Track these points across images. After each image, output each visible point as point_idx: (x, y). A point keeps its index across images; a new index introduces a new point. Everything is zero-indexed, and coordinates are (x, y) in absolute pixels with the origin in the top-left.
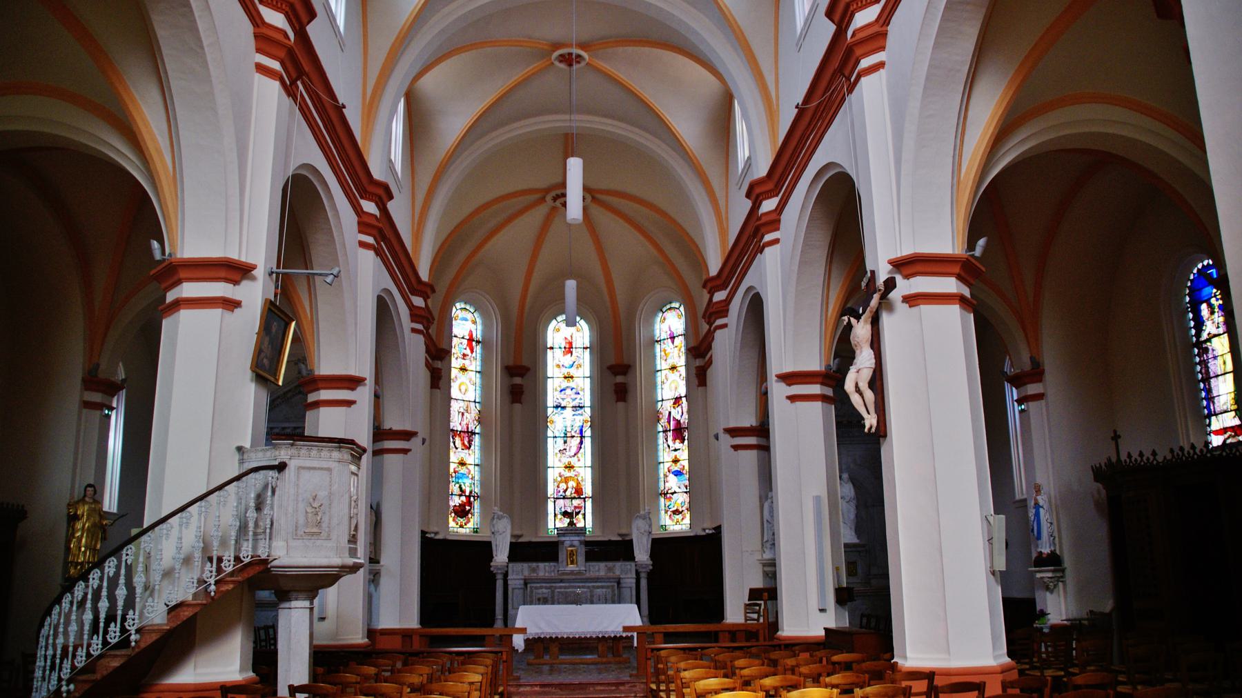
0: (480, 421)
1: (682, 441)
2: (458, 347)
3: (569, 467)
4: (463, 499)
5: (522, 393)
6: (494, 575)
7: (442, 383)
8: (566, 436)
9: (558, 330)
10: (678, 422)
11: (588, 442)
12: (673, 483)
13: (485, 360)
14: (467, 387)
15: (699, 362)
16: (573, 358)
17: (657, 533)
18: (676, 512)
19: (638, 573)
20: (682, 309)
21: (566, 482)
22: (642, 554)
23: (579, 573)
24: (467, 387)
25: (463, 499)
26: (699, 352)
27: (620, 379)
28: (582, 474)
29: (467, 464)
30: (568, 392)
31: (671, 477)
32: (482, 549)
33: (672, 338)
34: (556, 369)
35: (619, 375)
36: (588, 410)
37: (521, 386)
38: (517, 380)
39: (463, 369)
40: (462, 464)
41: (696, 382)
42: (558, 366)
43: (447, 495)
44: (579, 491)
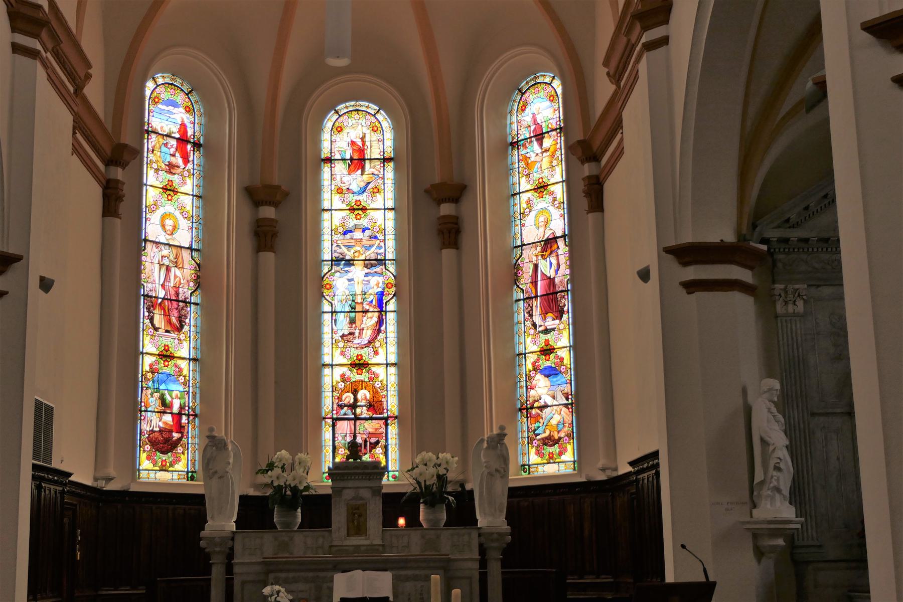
0: (199, 282)
1: (559, 314)
2: (157, 154)
3: (359, 365)
4: (168, 418)
5: (274, 235)
6: (208, 556)
7: (123, 208)
8: (353, 309)
9: (340, 130)
10: (551, 281)
11: (391, 318)
12: (542, 389)
13: (209, 178)
14: (172, 216)
15: (587, 169)
16: (366, 178)
17: (517, 478)
18: (549, 441)
19: (483, 550)
20: (557, 84)
21: (355, 393)
22: (491, 518)
23: (372, 549)
24: (172, 216)
25: (168, 418)
26: (589, 151)
27: (446, 209)
28: (382, 377)
29: (172, 362)
30: (358, 235)
31: (541, 381)
32: (185, 508)
33: (540, 137)
34: (336, 197)
35: (445, 205)
36: (392, 268)
37: (271, 222)
38: (268, 212)
39: (169, 190)
40: (166, 356)
41: (584, 203)
42: (340, 191)
43: (135, 411)
44: (375, 406)
